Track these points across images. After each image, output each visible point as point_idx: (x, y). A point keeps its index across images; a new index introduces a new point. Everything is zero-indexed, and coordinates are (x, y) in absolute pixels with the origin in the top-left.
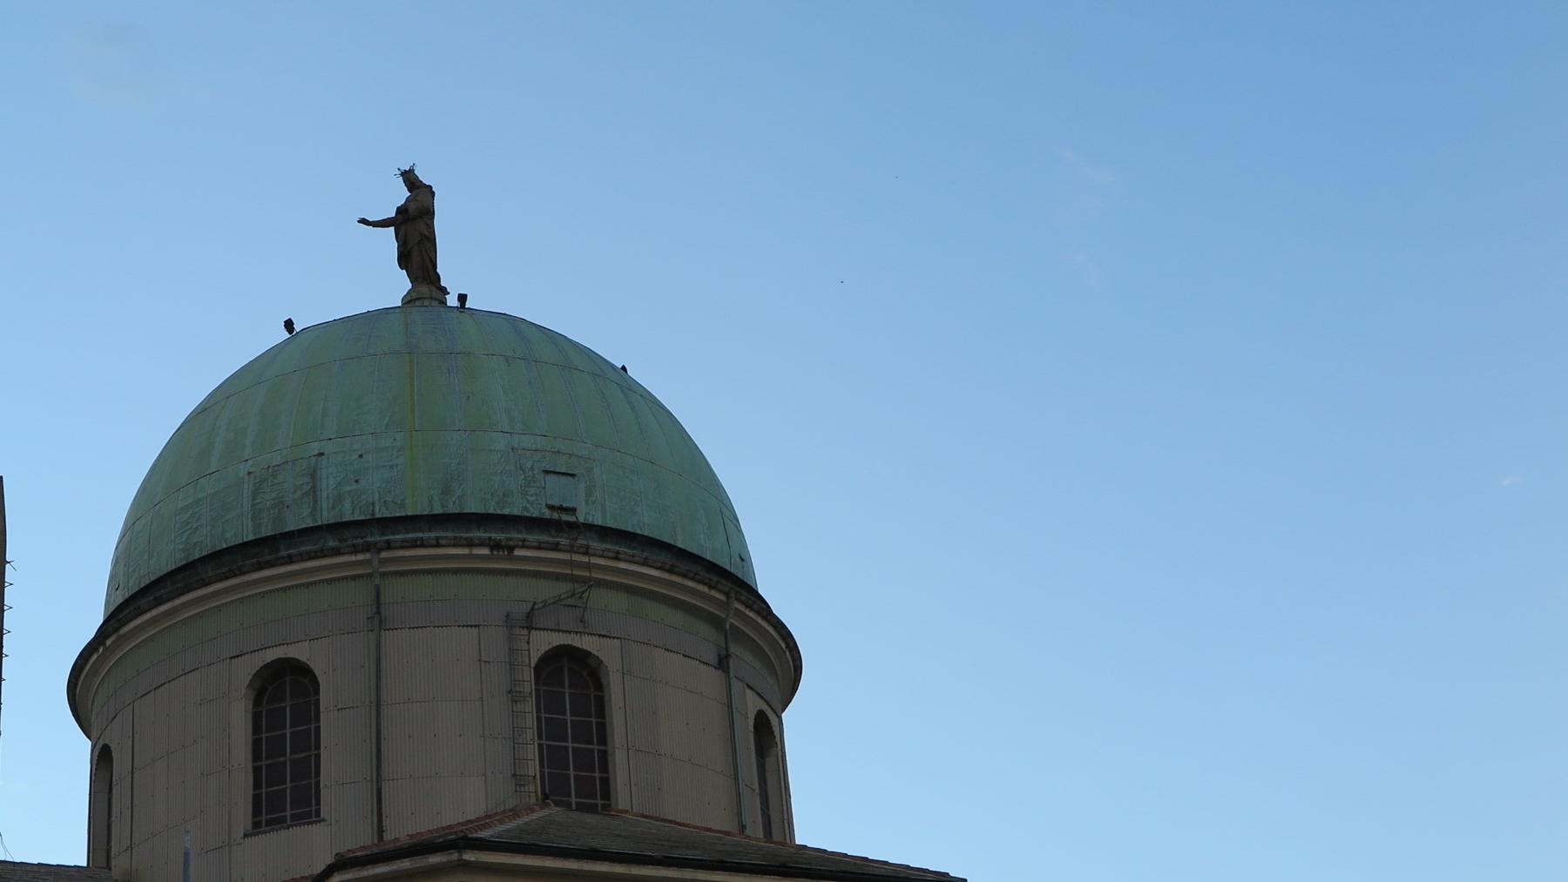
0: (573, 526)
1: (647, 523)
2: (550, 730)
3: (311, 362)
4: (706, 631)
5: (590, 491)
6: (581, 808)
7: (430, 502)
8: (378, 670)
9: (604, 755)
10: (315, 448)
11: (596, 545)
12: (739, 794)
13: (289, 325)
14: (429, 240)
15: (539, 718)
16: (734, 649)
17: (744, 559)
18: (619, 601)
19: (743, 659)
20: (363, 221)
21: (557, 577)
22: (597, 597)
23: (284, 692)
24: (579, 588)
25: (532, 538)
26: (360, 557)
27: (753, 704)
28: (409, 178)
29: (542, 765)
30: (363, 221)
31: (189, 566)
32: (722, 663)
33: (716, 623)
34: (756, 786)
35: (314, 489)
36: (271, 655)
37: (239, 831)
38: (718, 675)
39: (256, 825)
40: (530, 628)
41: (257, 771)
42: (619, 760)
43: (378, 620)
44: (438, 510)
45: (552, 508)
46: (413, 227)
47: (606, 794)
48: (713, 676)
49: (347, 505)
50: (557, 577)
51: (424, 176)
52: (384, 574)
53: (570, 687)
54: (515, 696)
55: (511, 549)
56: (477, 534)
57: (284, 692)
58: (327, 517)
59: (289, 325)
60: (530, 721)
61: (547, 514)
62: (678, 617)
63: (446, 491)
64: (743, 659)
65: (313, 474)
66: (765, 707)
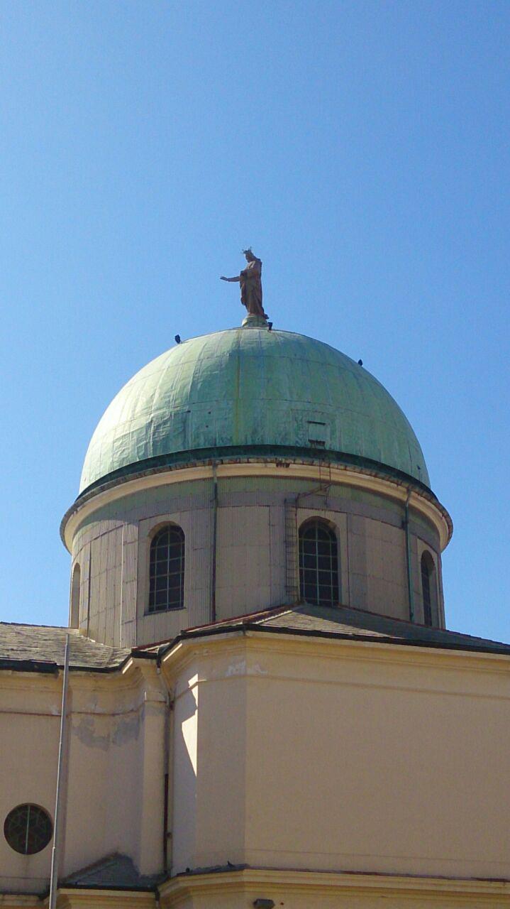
2: (306, 561)
5: (333, 432)
16: (411, 517)
20: (223, 278)
27: (421, 547)
28: (249, 256)
29: (301, 581)
30: (223, 278)
32: (404, 525)
35: (184, 430)
47: (337, 596)
54: (287, 544)
55: (288, 465)
61: (309, 445)
63: (255, 432)
65: (184, 422)
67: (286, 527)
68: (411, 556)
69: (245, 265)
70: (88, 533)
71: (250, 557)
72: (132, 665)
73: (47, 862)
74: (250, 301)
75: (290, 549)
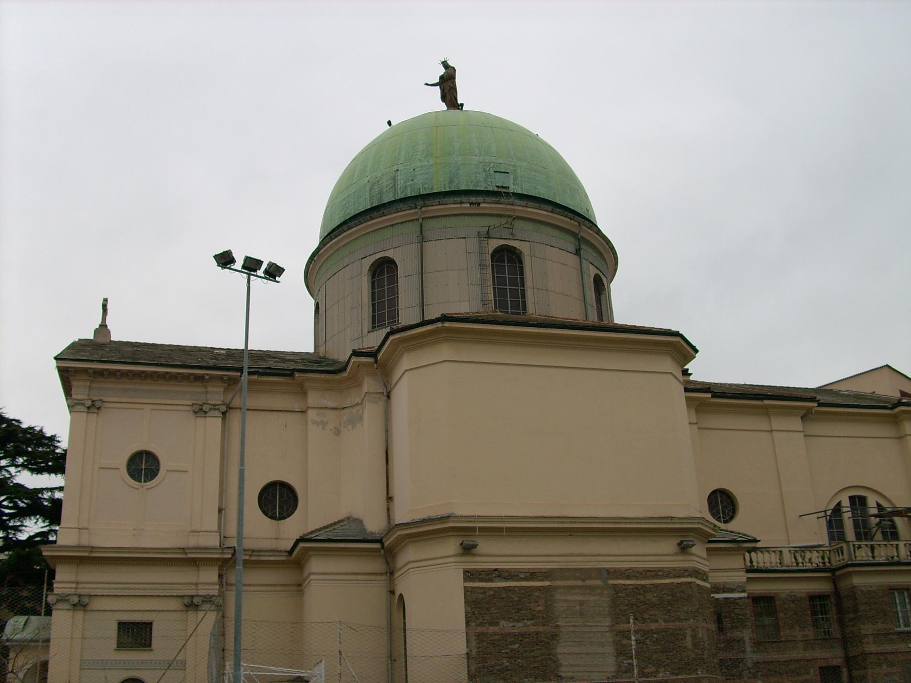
0: (507, 194)
1: (542, 192)
2: (498, 281)
3: (401, 139)
4: (571, 239)
5: (515, 179)
6: (512, 313)
7: (445, 186)
8: (783, 504)
9: (523, 291)
10: (395, 168)
11: (518, 202)
12: (586, 309)
13: (389, 123)
14: (454, 89)
15: (493, 276)
16: (583, 246)
17: (589, 209)
18: (529, 226)
19: (586, 251)
20: (427, 84)
21: (500, 216)
22: (518, 224)
23: (383, 270)
24: (510, 220)
25: (488, 199)
26: (413, 211)
27: (593, 271)
28: (445, 64)
29: (495, 296)
30: (427, 84)
31: (345, 223)
32: (578, 252)
33: (574, 235)
34: (595, 304)
35: (394, 185)
36: (378, 256)
37: (365, 331)
38: (576, 258)
39: (373, 328)
40: (489, 238)
41: (373, 305)
42: (529, 294)
43: (422, 240)
44: (448, 190)
45: (498, 187)
46: (447, 85)
47: (525, 308)
48: (575, 258)
49: (409, 190)
50: (500, 216)
51: (451, 63)
52: (423, 219)
53: (507, 261)
54: (482, 266)
55: (479, 204)
56: (464, 199)
57: (383, 270)
58: (400, 196)
59: (389, 123)
60: (489, 276)
61: (496, 189)
62: (556, 233)
63: (451, 182)
64: (586, 251)
65: (394, 179)
66: (599, 273)
67: (481, 253)
68: (585, 276)
69: (442, 71)
70: (646, 616)
71: (451, 276)
72: (612, 579)
73: (292, 528)
74: (448, 97)
75: (484, 271)
